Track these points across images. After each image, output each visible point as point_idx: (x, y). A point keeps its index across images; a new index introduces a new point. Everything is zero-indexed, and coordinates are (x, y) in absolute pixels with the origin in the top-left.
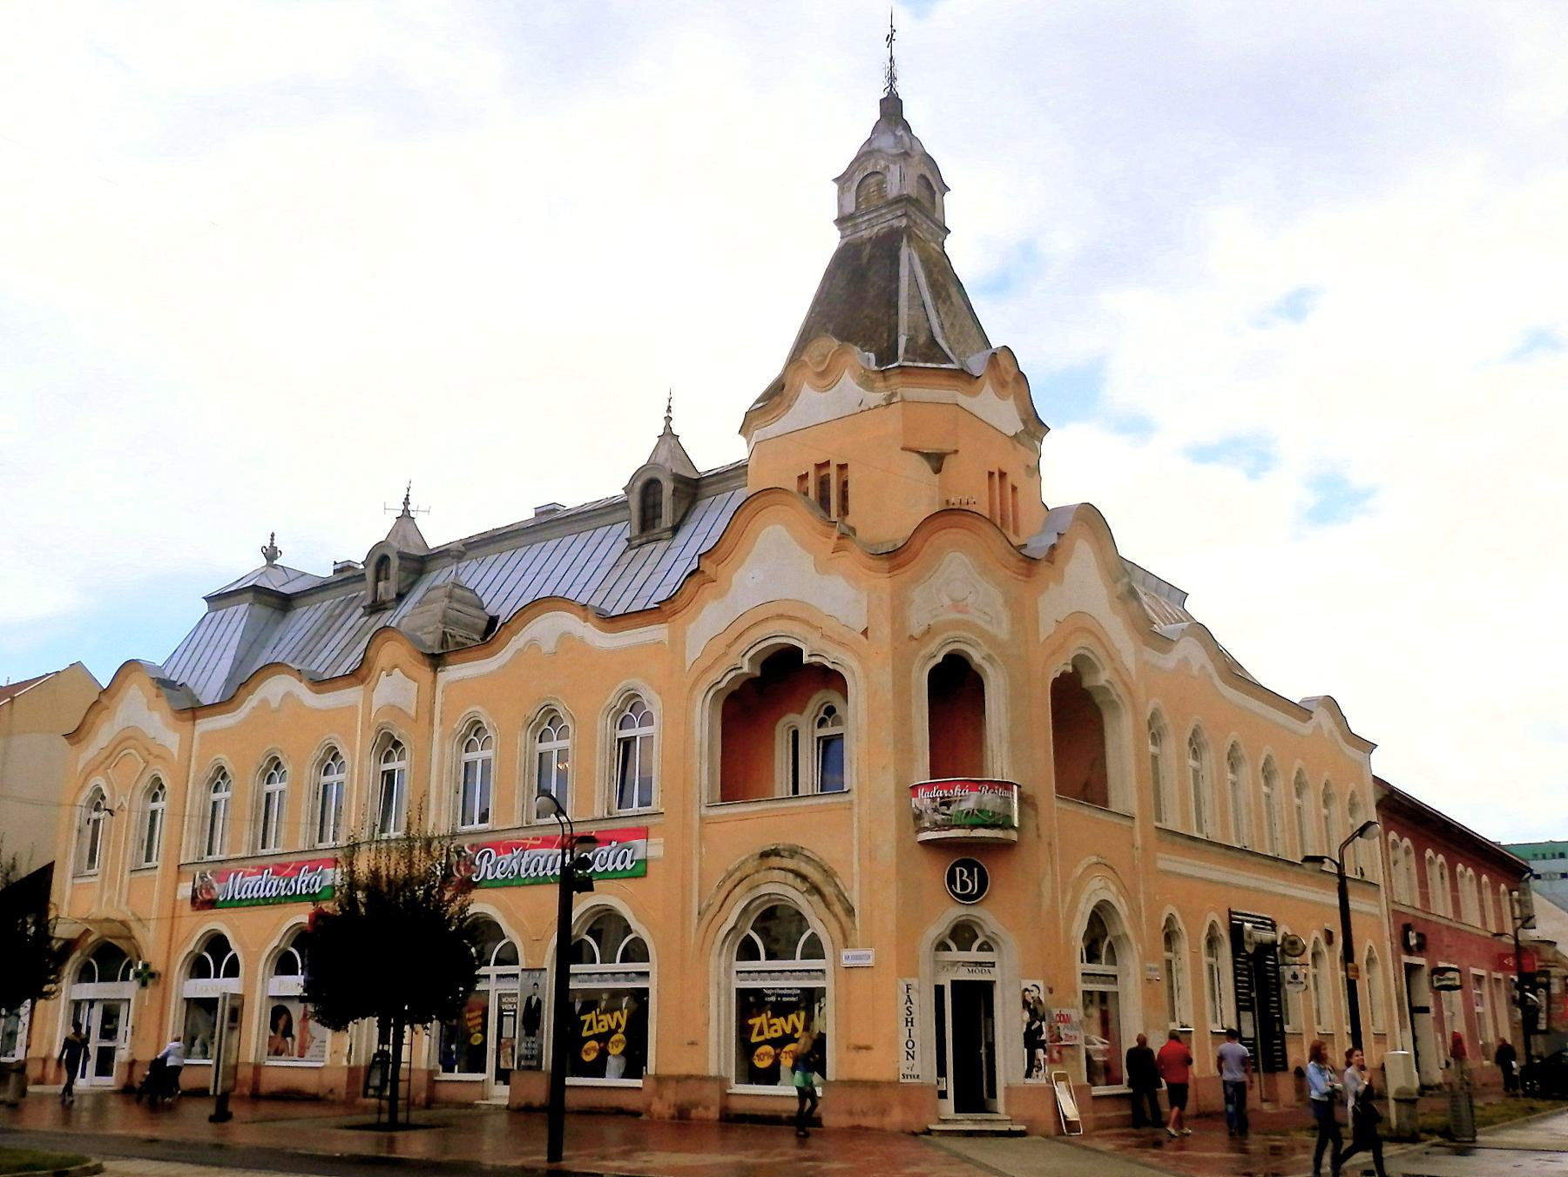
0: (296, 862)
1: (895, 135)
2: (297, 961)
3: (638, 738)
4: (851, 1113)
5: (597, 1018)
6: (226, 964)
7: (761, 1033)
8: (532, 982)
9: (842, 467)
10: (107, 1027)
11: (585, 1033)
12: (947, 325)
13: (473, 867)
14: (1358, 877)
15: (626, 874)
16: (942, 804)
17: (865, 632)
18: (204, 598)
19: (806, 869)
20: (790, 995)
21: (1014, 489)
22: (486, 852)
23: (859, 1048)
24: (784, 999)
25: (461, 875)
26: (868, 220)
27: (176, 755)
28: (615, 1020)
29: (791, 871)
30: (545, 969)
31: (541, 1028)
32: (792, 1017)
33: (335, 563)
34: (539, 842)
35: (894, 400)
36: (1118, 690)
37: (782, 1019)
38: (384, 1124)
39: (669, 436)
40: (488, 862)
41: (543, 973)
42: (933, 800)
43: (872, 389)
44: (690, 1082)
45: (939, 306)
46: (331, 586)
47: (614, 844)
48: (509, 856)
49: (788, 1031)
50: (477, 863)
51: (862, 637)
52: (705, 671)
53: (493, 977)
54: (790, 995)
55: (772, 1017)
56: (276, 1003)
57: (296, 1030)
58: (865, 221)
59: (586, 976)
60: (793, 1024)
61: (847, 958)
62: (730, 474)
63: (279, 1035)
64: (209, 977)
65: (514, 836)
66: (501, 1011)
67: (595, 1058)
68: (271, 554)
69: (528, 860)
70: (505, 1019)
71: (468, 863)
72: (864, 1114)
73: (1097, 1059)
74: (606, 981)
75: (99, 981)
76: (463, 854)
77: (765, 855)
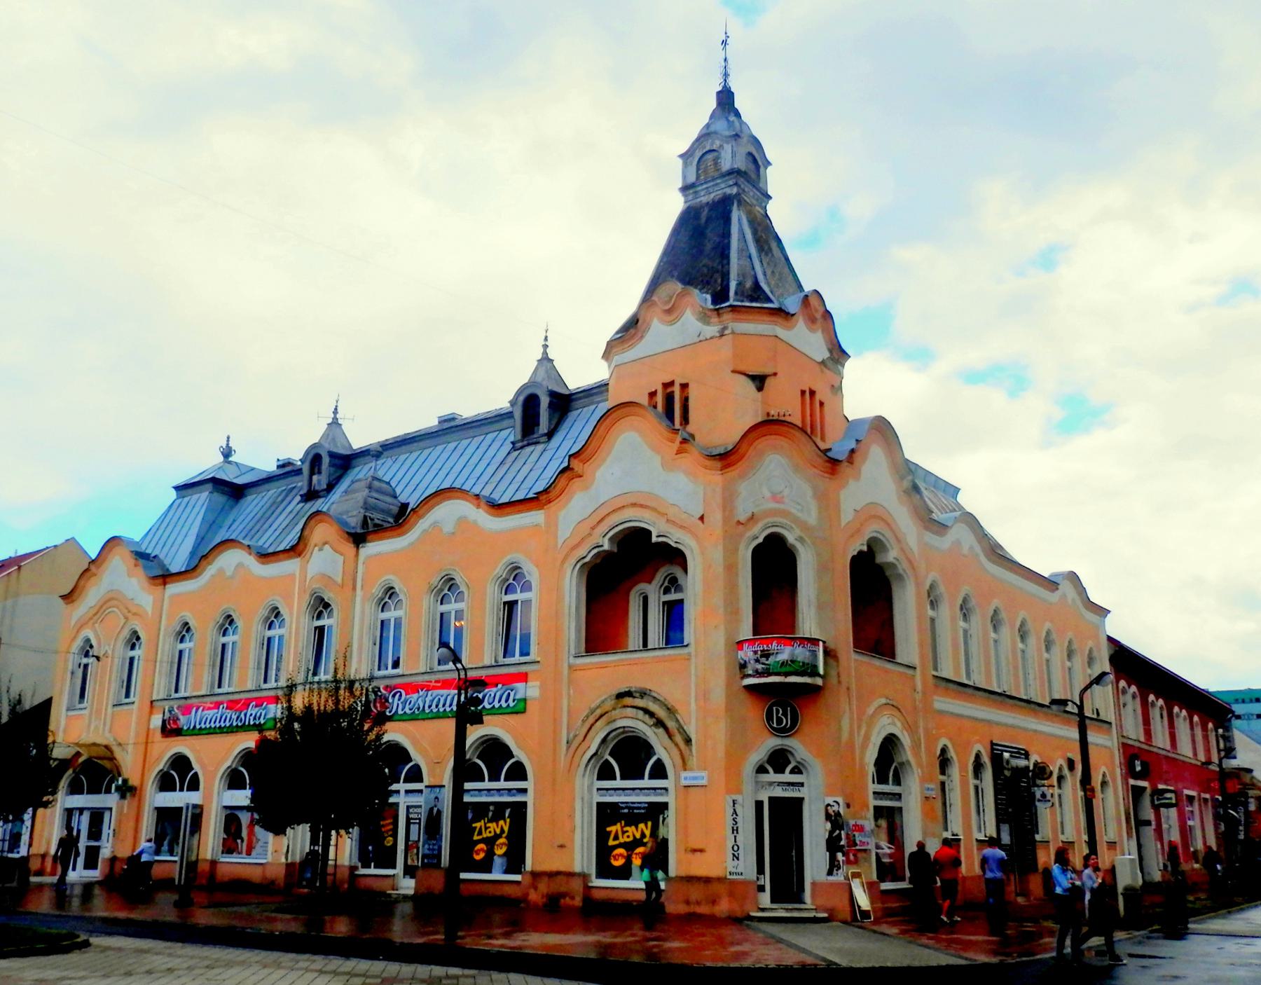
1: (728, 120)
4: (688, 902)
7: (616, 838)
8: (433, 796)
9: (684, 386)
11: (476, 838)
12: (769, 273)
13: (387, 704)
14: (1095, 716)
15: (509, 710)
16: (762, 656)
17: (702, 518)
21: (822, 404)
23: (694, 851)
26: (707, 188)
28: (640, 830)
33: (278, 460)
34: (439, 685)
35: (726, 332)
36: (903, 567)
37: (633, 827)
40: (399, 700)
42: (755, 652)
43: (708, 323)
44: (560, 877)
45: (763, 257)
47: (500, 686)
48: (415, 696)
49: (638, 836)
50: (390, 700)
51: (700, 522)
53: (402, 792)
55: (626, 825)
56: (229, 812)
58: (703, 190)
61: (686, 778)
68: (227, 453)
70: (412, 826)
72: (698, 903)
77: (620, 696)
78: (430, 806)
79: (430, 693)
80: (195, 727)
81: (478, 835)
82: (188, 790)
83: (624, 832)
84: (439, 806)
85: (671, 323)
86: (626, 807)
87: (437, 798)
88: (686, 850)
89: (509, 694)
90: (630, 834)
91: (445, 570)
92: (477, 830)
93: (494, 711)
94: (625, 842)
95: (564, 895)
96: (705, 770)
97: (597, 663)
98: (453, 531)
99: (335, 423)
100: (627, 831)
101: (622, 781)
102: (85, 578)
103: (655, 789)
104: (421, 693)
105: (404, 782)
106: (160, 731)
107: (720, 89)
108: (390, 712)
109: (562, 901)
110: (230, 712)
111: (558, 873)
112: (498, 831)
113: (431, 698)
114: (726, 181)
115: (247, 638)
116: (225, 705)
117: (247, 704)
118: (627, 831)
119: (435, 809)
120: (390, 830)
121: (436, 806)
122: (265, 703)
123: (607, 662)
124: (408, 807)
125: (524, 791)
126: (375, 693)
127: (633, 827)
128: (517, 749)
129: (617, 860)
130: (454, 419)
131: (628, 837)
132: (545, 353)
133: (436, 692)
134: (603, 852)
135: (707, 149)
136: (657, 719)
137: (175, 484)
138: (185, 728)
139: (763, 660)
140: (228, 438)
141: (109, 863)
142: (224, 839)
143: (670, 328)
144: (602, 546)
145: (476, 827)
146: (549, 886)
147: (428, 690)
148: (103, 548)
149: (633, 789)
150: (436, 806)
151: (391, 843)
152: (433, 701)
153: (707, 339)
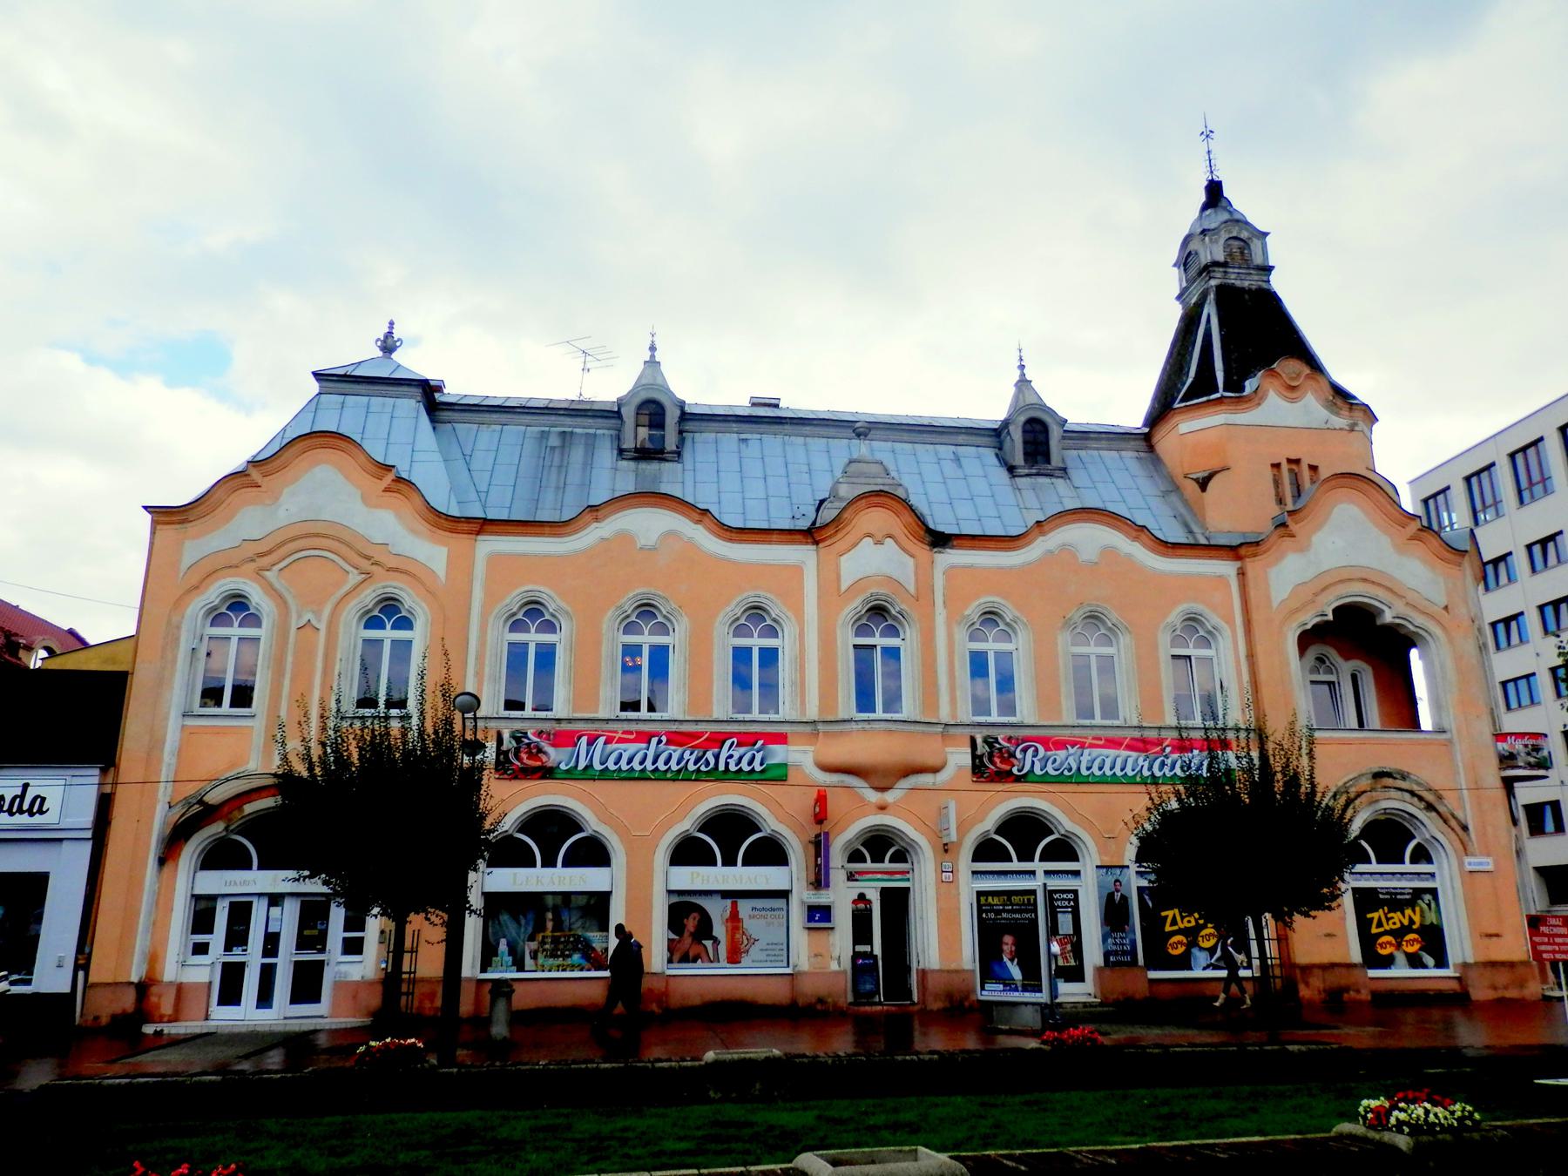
0: (711, 733)
3: (879, 648)
4: (1495, 988)
5: (1386, 917)
7: (1380, 924)
8: (1111, 879)
10: (307, 932)
11: (1168, 928)
13: (1012, 759)
16: (1533, 750)
17: (1446, 608)
18: (315, 374)
19: (1415, 788)
20: (1404, 894)
22: (1030, 746)
23: (1490, 936)
24: (1399, 897)
25: (997, 767)
26: (1239, 273)
28: (1407, 917)
29: (1407, 791)
30: (1128, 867)
31: (1131, 923)
32: (1408, 912)
34: (632, 737)
35: (1356, 428)
37: (1399, 913)
39: (1023, 383)
41: (1125, 870)
42: (1526, 746)
43: (1337, 414)
44: (1337, 970)
46: (815, 422)
49: (1406, 922)
50: (1019, 755)
51: (1444, 612)
52: (1297, 610)
53: (1040, 874)
54: (1404, 894)
55: (1389, 912)
56: (675, 899)
57: (719, 930)
58: (1235, 273)
59: (1390, 876)
60: (1410, 917)
61: (1470, 864)
62: (1092, 435)
63: (688, 940)
64: (555, 866)
65: (1064, 734)
67: (1182, 953)
68: (388, 346)
69: (1089, 758)
71: (1006, 755)
72: (1506, 988)
73: (595, 934)
76: (526, 741)
77: (1378, 775)
79: (1086, 751)
80: (589, 767)
81: (1171, 925)
82: (745, 864)
83: (1388, 919)
84: (1123, 891)
85: (1293, 400)
86: (1387, 893)
88: (1481, 936)
90: (1396, 920)
91: (1089, 605)
94: (1391, 929)
95: (1347, 989)
96: (1488, 855)
97: (1338, 739)
98: (1096, 560)
99: (1023, 383)
100: (1392, 918)
101: (565, 869)
103: (1419, 874)
105: (1041, 860)
108: (1019, 771)
109: (1346, 995)
110: (1134, 754)
111: (1333, 966)
114: (1261, 275)
116: (664, 739)
117: (718, 740)
118: (1392, 918)
121: (1118, 891)
122: (760, 743)
123: (1349, 739)
125: (1076, 873)
127: (1399, 913)
128: (985, 823)
129: (1385, 948)
130: (776, 406)
131: (1394, 923)
132: (653, 356)
133: (1096, 752)
134: (1367, 940)
135: (1234, 234)
136: (1427, 802)
137: (321, 366)
138: (563, 767)
139: (1534, 754)
140: (392, 324)
141: (379, 988)
142: (670, 941)
143: (1289, 404)
144: (1326, 615)
145: (1167, 917)
146: (1324, 981)
148: (300, 436)
149: (1393, 874)
153: (1335, 429)
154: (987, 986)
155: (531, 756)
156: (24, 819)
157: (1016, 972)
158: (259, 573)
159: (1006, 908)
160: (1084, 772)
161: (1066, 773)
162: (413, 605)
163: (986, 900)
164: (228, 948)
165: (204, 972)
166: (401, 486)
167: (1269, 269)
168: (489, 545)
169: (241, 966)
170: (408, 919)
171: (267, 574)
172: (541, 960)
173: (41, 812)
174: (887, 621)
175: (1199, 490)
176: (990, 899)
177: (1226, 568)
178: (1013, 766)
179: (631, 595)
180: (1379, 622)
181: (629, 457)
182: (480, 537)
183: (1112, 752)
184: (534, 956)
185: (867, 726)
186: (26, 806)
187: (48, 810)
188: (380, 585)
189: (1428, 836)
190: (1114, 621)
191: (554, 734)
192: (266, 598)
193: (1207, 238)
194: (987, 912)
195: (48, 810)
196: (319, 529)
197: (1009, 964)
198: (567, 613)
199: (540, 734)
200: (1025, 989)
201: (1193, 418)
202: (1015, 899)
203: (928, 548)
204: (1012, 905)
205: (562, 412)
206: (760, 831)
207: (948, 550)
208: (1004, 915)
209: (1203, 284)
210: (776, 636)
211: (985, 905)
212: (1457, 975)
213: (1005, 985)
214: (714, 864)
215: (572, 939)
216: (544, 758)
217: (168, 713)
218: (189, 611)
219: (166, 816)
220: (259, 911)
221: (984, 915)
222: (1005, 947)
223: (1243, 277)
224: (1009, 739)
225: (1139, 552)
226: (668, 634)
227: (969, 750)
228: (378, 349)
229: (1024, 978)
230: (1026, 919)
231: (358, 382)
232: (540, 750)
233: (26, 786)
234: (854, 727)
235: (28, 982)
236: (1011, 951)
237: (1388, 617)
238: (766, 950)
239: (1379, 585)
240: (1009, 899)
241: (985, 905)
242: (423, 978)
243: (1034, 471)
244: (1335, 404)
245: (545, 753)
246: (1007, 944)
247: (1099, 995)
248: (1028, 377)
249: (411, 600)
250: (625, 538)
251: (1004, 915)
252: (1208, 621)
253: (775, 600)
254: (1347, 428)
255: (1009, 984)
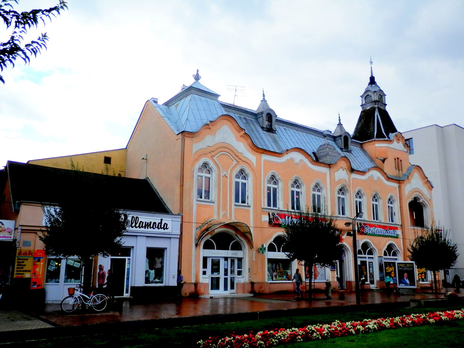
2: (274, 245)
6: (387, 254)
8: (380, 260)
15: (395, 237)
17: (430, 200)
21: (401, 161)
25: (275, 222)
27: (255, 164)
33: (184, 85)
34: (378, 226)
38: (434, 293)
39: (264, 100)
40: (368, 229)
43: (405, 148)
46: (299, 127)
47: (392, 230)
48: (372, 228)
50: (365, 228)
53: (367, 258)
66: (369, 266)
68: (197, 77)
70: (370, 268)
71: (277, 219)
74: (390, 260)
75: (231, 250)
78: (380, 263)
79: (376, 228)
87: (381, 260)
89: (395, 233)
92: (387, 270)
93: (372, 235)
98: (376, 180)
99: (264, 100)
102: (295, 150)
104: (374, 228)
106: (268, 223)
107: (371, 76)
112: (392, 270)
113: (376, 230)
115: (382, 206)
119: (381, 263)
120: (365, 269)
124: (369, 262)
126: (273, 215)
140: (198, 70)
147: (375, 227)
150: (381, 263)
151: (366, 274)
152: (377, 231)
154: (400, 285)
155: (277, 221)
156: (162, 231)
157: (408, 281)
158: (212, 157)
159: (405, 267)
160: (376, 233)
161: (373, 233)
162: (249, 173)
163: (400, 265)
164: (212, 272)
165: (206, 280)
166: (245, 136)
167: (386, 105)
168: (265, 157)
169: (218, 279)
170: (440, 271)
171: (214, 158)
172: (277, 278)
173: (167, 228)
174: (207, 168)
175: (382, 163)
176: (401, 265)
177: (396, 185)
178: (364, 231)
179: (294, 177)
180: (418, 201)
181: (265, 130)
182: (262, 155)
183: (380, 229)
184: (276, 277)
185: (343, 219)
186: (162, 227)
187: (168, 228)
188: (241, 165)
189: (396, 249)
190: (380, 196)
191: (281, 215)
192: (214, 166)
193: (375, 94)
194: (400, 268)
195: (168, 228)
196: (226, 146)
197: (406, 280)
198: (281, 180)
199: (278, 214)
200: (410, 285)
201: (379, 143)
202: (407, 265)
203: (350, 172)
204: (407, 266)
205: (242, 111)
206: (235, 240)
207: (353, 174)
208: (405, 269)
209: (372, 105)
210: (344, 195)
211: (399, 266)
212: (430, 283)
213: (405, 284)
214: (214, 249)
215: (284, 272)
216: (279, 222)
217: (193, 199)
218: (196, 166)
219: (196, 232)
220: (222, 262)
221: (399, 268)
222: (405, 276)
223: (381, 106)
224: (364, 224)
225: (383, 178)
226: (299, 189)
227: (268, 217)
228: (194, 78)
229: (410, 283)
230: (410, 270)
231: (202, 92)
232: (278, 219)
233: (162, 220)
234: (340, 218)
235: (162, 282)
236: (406, 277)
237: (421, 201)
238: (321, 276)
239: (421, 193)
240: (406, 265)
241: (399, 266)
242: (259, 282)
243: (346, 150)
244: (405, 145)
245: (279, 220)
246: (405, 275)
247: (379, 288)
248: (266, 100)
249: (248, 171)
250: (292, 160)
251: (405, 269)
252: (394, 198)
253: (247, 167)
254: (406, 152)
255: (406, 284)
